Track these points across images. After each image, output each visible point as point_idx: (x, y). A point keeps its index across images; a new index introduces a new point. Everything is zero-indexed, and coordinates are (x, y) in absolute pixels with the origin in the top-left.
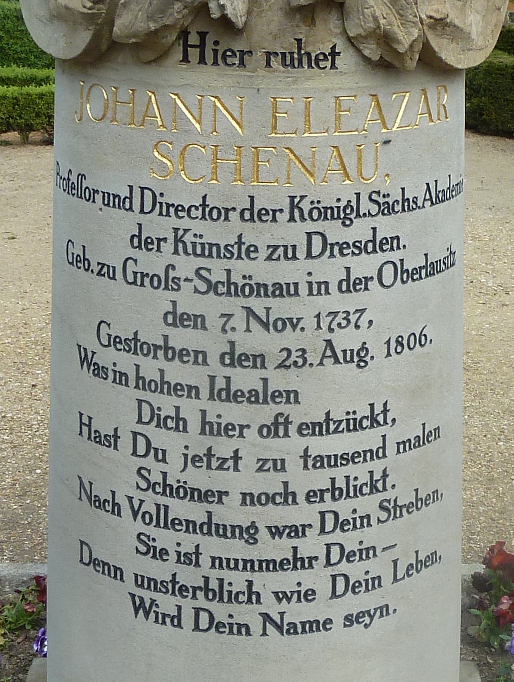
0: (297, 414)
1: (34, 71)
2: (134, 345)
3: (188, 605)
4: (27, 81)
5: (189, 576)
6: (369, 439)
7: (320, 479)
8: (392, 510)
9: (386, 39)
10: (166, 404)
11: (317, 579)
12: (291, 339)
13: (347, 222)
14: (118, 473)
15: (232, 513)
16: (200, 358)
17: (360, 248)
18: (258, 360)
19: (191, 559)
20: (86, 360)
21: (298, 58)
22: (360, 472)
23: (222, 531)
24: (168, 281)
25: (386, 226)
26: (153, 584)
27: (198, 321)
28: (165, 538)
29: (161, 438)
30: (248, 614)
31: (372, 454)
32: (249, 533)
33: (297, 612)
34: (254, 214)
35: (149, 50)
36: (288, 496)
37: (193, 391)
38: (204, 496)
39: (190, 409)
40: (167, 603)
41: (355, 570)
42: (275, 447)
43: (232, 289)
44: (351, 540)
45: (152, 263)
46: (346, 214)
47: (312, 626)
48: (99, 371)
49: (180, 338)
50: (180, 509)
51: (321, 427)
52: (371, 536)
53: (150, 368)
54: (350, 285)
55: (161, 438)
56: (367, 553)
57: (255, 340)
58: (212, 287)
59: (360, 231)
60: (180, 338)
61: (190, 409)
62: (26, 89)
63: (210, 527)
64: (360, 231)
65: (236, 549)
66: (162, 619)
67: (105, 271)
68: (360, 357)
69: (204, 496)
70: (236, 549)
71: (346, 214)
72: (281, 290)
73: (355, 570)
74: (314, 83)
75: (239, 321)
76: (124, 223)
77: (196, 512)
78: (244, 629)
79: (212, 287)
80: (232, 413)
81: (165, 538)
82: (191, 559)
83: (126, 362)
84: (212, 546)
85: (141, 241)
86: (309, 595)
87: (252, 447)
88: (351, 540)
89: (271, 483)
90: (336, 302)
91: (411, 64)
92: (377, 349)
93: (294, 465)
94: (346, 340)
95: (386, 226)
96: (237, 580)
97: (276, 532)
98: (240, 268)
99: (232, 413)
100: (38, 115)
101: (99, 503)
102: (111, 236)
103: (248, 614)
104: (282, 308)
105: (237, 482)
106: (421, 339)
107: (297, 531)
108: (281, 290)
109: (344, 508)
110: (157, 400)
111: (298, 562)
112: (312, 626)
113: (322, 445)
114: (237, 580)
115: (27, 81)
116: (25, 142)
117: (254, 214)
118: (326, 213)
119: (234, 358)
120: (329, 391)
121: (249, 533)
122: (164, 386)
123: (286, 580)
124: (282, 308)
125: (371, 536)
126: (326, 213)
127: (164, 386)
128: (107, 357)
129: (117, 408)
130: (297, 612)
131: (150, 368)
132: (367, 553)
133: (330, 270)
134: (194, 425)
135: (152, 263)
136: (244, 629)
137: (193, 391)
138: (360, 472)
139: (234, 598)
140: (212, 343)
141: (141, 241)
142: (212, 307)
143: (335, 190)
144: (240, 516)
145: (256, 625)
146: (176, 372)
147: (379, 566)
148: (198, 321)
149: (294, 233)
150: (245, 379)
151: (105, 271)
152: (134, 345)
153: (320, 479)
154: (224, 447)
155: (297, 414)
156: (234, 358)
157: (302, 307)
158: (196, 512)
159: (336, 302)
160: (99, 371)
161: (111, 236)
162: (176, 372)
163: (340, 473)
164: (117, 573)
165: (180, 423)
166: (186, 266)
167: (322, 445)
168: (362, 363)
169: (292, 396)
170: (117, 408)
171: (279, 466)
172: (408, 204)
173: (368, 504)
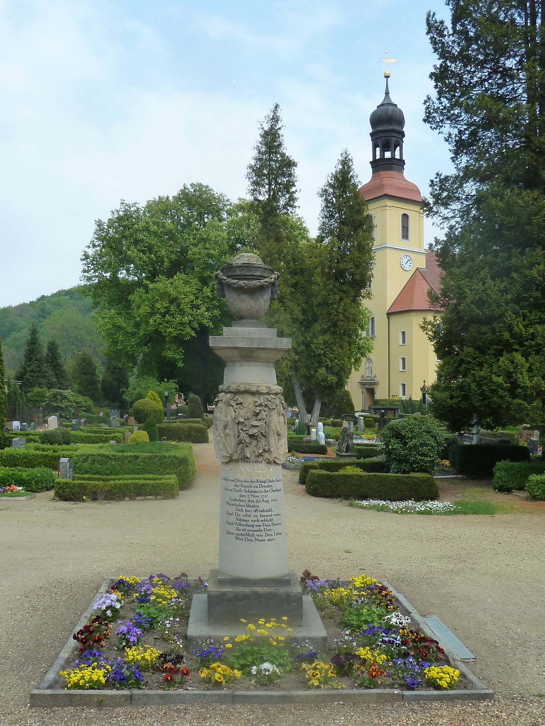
0: (259, 509)
1: (157, 476)
2: (235, 500)
3: (244, 537)
4: (156, 479)
5: (244, 533)
6: (270, 513)
7: (263, 519)
8: (274, 524)
9: (269, 460)
10: (240, 508)
11: (263, 533)
12: (257, 498)
13: (265, 483)
14: (233, 519)
15: (250, 523)
16: (245, 501)
17: (267, 487)
18: (253, 501)
19: (244, 530)
20: (228, 503)
21: (257, 462)
22: (268, 518)
23: (249, 526)
24: (240, 491)
25: (270, 484)
26: (239, 535)
27: (245, 496)
28: (240, 527)
29: (239, 513)
30: (253, 538)
31: (270, 516)
32: (253, 526)
33: (260, 538)
34: (252, 482)
35: (237, 461)
36: (258, 521)
37: (244, 506)
38: (246, 521)
39: (244, 508)
40: (241, 537)
41: (269, 533)
42: (256, 514)
43: (249, 492)
44: (268, 528)
45: (238, 489)
46: (264, 482)
47: (263, 540)
48: (230, 504)
49: (242, 499)
50: (242, 523)
51: (262, 511)
52: (271, 528)
53: (238, 503)
54: (265, 491)
55: (239, 513)
56: (270, 530)
57: (252, 499)
58: (246, 491)
59: (267, 484)
60: (242, 499)
61: (244, 508)
62: (156, 481)
63: (247, 525)
64: (267, 484)
65: (251, 528)
66: (240, 540)
67: (231, 490)
68: (268, 501)
69: (246, 521)
70: (251, 528)
71: (264, 482)
72: (256, 492)
73: (269, 533)
74: (259, 465)
75: (250, 496)
76: (234, 483)
77: (245, 523)
78: (252, 540)
79: (246, 491)
80: (250, 509)
81: (240, 527)
82: (244, 530)
83: (234, 502)
84: (247, 528)
85: (236, 486)
86: (262, 536)
87: (253, 513)
88: (268, 528)
89: (256, 519)
90: (263, 494)
91: (272, 462)
92: (270, 500)
93: (259, 516)
94: (265, 499)
95: (270, 484)
96: (251, 533)
97: (256, 526)
98: (250, 489)
99: (250, 509)
100: (161, 490)
101: (230, 524)
102: (232, 485)
103: (253, 538)
104: (256, 494)
105: (251, 519)
106: (277, 500)
107: (259, 526)
108: (256, 492)
109: (266, 523)
110: (239, 507)
111: (260, 530)
112: (263, 540)
113: (262, 514)
114: (251, 533)
115: (154, 479)
116: (156, 499)
117: (252, 482)
118: (261, 482)
119: (249, 501)
120: (263, 506)
121: (253, 526)
122: (240, 505)
123: (258, 533)
124: (256, 494)
125: (271, 528)
126: (261, 482)
127: (240, 505)
128: (231, 502)
129: (233, 509)
130: (260, 538)
131: (238, 503)
132: (270, 530)
133: (263, 489)
134: (244, 511)
135: (238, 489)
136: (252, 540)
137: (244, 506)
138: (268, 518)
139: (251, 536)
140: (247, 499)
141: (236, 486)
142: (246, 494)
143: (264, 479)
144: (252, 524)
145: (254, 540)
146: (242, 503)
147: (272, 532)
148: (245, 496)
149: (258, 484)
150: (251, 504)
151: (231, 490)
152: (235, 500)
153: (263, 519)
154: (249, 514)
155: (259, 509)
156: (249, 501)
157: (259, 494)
158: (245, 523)
159: (263, 494)
160: (230, 504)
161: (232, 485)
162: (242, 503)
163: (265, 518)
164: (233, 534)
165: (242, 510)
166: (243, 489)
167: (262, 514)
168: (268, 502)
169: (258, 506)
170: (233, 509)
171: (257, 516)
172: (273, 481)
173: (270, 523)
